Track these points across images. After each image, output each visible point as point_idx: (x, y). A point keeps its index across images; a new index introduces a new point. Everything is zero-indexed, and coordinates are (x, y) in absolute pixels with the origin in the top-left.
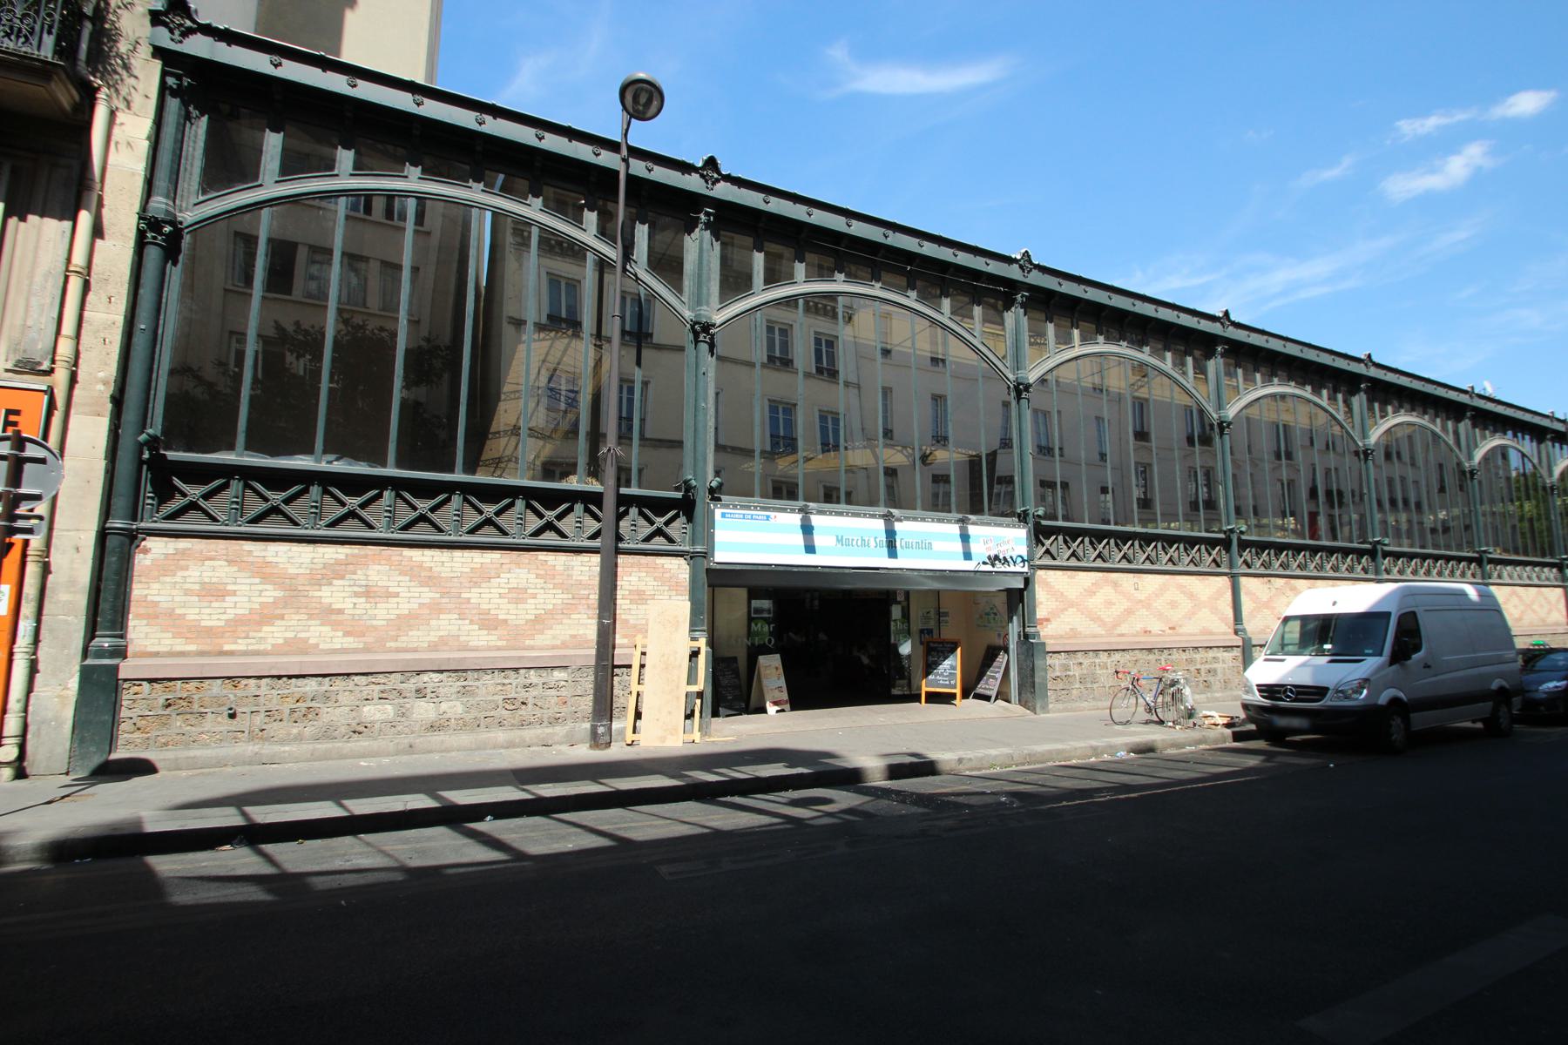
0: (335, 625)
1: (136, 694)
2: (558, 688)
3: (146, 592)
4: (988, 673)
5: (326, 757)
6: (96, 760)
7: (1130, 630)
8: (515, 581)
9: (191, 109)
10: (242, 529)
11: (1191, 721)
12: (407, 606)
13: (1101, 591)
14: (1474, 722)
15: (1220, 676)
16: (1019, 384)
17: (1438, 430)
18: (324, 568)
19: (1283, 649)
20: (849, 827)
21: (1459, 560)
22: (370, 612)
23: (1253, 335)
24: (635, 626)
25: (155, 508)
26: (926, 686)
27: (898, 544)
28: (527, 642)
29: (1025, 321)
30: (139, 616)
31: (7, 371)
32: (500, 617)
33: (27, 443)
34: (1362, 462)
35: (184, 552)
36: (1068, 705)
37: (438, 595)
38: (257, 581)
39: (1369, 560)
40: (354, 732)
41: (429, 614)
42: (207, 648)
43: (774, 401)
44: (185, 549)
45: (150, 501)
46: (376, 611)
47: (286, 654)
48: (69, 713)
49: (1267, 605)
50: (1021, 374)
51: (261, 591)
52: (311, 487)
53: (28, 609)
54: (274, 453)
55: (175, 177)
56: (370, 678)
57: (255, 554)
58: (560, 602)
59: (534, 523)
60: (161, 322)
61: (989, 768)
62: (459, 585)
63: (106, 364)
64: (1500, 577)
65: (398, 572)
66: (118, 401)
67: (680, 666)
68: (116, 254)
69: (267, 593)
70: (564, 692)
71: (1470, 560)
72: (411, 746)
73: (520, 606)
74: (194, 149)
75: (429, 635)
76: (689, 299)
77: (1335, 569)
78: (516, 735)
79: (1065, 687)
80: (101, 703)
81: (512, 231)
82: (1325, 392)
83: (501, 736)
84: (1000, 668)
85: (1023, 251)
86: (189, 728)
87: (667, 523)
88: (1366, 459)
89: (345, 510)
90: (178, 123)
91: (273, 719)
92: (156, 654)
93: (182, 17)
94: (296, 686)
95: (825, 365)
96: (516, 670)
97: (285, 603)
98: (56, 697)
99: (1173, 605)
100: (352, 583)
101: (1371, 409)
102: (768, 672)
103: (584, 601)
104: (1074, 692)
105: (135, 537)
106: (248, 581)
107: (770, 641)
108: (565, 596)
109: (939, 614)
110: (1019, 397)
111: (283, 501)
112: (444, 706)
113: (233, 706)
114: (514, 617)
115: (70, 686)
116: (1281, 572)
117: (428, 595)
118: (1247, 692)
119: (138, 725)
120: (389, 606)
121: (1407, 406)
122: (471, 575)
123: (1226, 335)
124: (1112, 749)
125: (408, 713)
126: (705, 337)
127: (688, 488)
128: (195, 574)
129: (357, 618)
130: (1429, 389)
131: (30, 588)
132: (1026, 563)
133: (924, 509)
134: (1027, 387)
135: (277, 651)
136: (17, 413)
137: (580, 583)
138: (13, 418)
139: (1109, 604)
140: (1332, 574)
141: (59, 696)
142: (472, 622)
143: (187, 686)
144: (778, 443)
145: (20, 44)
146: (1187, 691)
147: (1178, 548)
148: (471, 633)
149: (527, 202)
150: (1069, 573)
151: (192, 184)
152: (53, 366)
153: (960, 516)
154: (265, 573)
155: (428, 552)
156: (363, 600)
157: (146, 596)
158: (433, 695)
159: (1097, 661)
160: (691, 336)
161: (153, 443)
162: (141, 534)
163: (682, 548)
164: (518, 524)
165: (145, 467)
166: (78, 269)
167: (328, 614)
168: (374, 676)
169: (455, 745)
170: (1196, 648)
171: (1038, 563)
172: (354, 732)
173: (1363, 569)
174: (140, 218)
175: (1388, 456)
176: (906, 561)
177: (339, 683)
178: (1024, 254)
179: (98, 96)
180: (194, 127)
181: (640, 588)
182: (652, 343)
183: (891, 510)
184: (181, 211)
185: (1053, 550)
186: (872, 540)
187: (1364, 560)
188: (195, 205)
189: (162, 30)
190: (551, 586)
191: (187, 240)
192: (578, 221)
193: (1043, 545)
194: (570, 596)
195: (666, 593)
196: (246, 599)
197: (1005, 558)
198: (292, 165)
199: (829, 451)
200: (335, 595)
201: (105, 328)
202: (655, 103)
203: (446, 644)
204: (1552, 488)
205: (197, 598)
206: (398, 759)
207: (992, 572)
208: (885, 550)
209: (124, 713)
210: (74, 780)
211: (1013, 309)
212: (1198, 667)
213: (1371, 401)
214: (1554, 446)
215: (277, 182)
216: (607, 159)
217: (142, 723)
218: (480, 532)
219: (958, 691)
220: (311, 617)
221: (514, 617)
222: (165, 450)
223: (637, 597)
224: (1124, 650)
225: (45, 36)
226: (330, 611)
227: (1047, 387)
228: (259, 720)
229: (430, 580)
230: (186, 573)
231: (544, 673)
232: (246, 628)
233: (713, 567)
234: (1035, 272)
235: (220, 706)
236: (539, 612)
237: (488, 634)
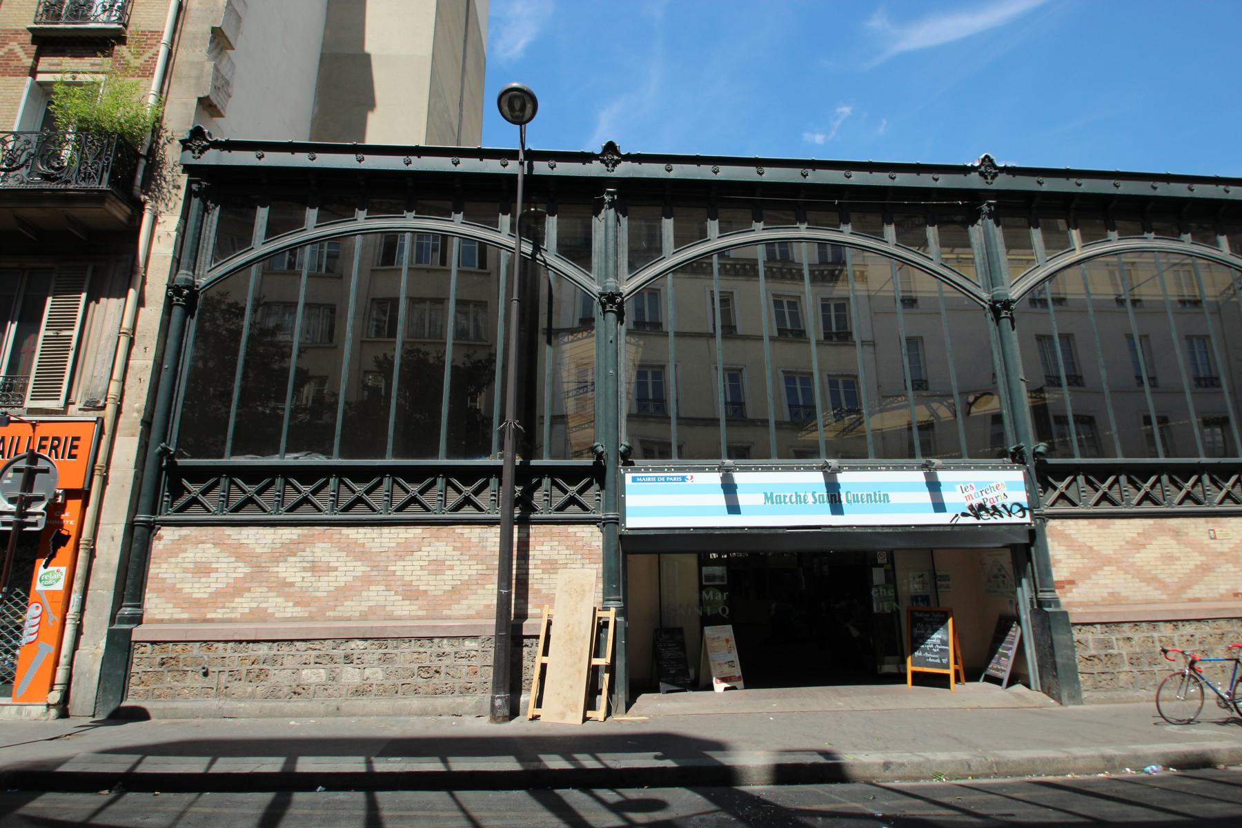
0: (288, 596)
1: (142, 653)
2: (469, 657)
4: (1000, 650)
5: (270, 715)
8: (435, 553)
9: (208, 203)
12: (344, 579)
13: (1154, 542)
16: (995, 302)
18: (282, 547)
22: (315, 584)
27: (843, 498)
28: (446, 612)
29: (998, 233)
30: (152, 590)
32: (422, 588)
33: (39, 459)
36: (1114, 694)
37: (369, 569)
38: (233, 559)
40: (295, 693)
41: (361, 586)
42: (195, 616)
43: (789, 372)
44: (186, 536)
45: (166, 499)
46: (320, 584)
48: (97, 667)
50: (999, 291)
51: (236, 568)
53: (77, 585)
56: (309, 645)
57: (233, 537)
59: (453, 498)
61: (931, 778)
67: (584, 638)
68: (152, 315)
72: (338, 709)
73: (439, 577)
79: (1107, 670)
80: (119, 660)
83: (415, 703)
84: (1012, 643)
85: (983, 156)
86: (176, 683)
87: (580, 492)
90: (198, 215)
91: (235, 678)
92: (161, 621)
94: (252, 650)
95: (834, 330)
96: (431, 639)
100: (301, 559)
102: (716, 644)
105: (153, 528)
106: (226, 560)
107: (724, 610)
108: (480, 567)
111: (256, 493)
112: (368, 672)
113: (206, 666)
114: (433, 588)
117: (360, 568)
120: (330, 579)
122: (396, 549)
124: (1139, 761)
126: (611, 307)
128: (191, 555)
129: (304, 589)
131: (80, 571)
132: (1027, 513)
133: (878, 456)
135: (245, 619)
136: (78, 439)
138: (76, 443)
141: (93, 654)
142: (397, 593)
148: (396, 603)
155: (362, 530)
156: (309, 574)
157: (158, 574)
158: (358, 661)
159: (1156, 635)
167: (283, 587)
174: (168, 288)
176: (854, 517)
177: (285, 648)
178: (983, 160)
180: (210, 216)
183: (828, 461)
185: (1071, 494)
188: (209, 271)
189: (189, 153)
190: (467, 557)
192: (1215, 244)
193: (1055, 488)
195: (578, 561)
197: (994, 508)
198: (682, 241)
200: (289, 571)
202: (529, 107)
203: (374, 613)
205: (190, 575)
206: (325, 720)
207: (977, 525)
208: (827, 505)
209: (134, 669)
211: (980, 222)
215: (263, 244)
217: (145, 678)
218: (189, 510)
220: (270, 589)
221: (433, 588)
224: (1199, 620)
225: (105, 173)
227: (1066, 305)
228: (224, 678)
229: (361, 554)
230: (184, 555)
231: (456, 642)
233: (625, 533)
235: (198, 665)
236: (455, 583)
237: (410, 605)
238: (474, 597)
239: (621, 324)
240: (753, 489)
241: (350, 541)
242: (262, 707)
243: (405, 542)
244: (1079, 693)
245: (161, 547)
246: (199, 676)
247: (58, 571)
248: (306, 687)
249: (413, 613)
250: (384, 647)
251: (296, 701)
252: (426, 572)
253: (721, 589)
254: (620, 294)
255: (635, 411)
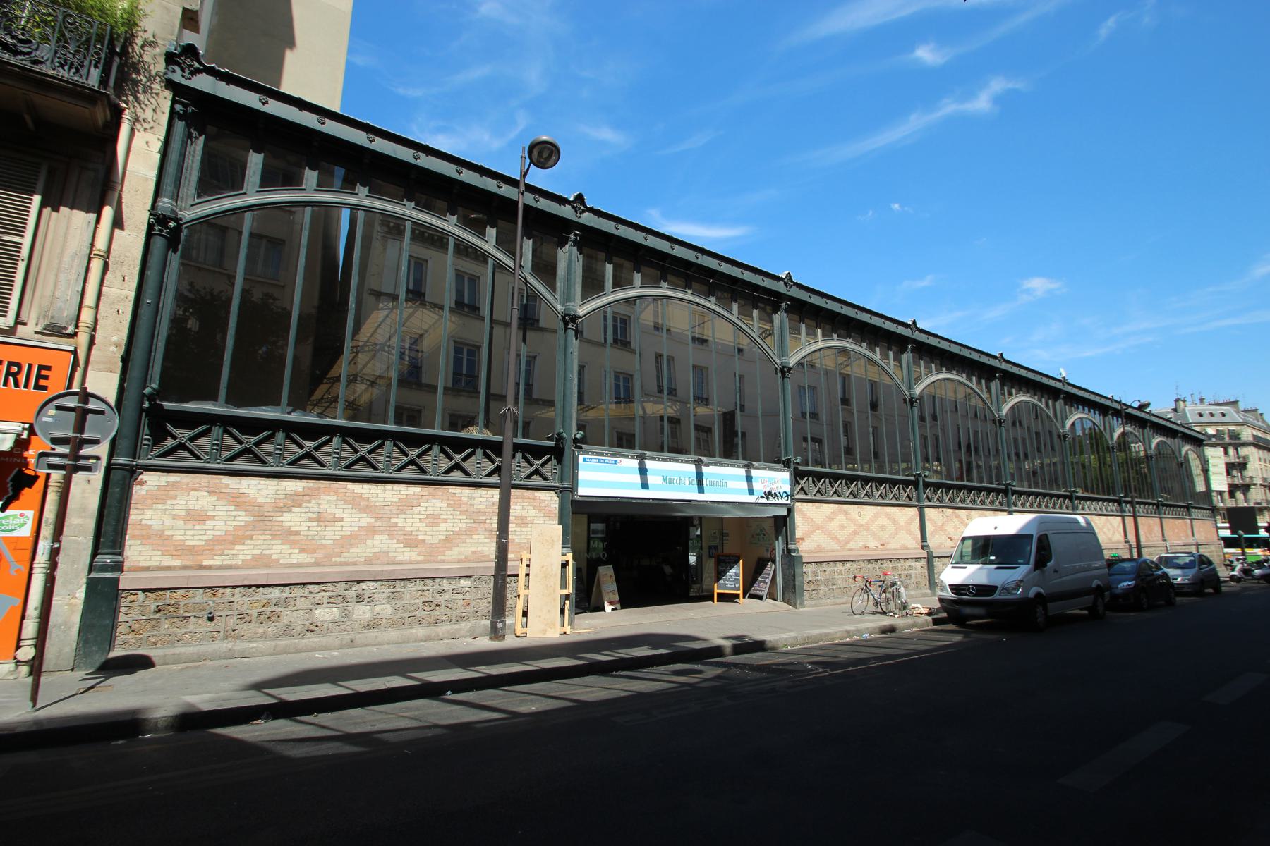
0: (293, 544)
2: (463, 593)
3: (141, 517)
4: (760, 579)
6: (99, 660)
7: (856, 546)
9: (192, 130)
10: (221, 466)
11: (905, 611)
12: (349, 528)
14: (1081, 609)
15: (913, 579)
16: (784, 367)
17: (1043, 406)
18: (286, 498)
19: (961, 559)
20: (722, 687)
21: (1058, 496)
22: (320, 533)
23: (931, 338)
24: (519, 544)
25: (150, 448)
26: (718, 589)
28: (440, 557)
29: (786, 321)
30: (133, 537)
31: (36, 333)
32: (420, 537)
33: (90, 398)
34: (998, 428)
35: (173, 484)
37: (373, 520)
38: (232, 508)
39: (1004, 496)
40: (308, 631)
42: (189, 563)
43: (618, 372)
47: (254, 568)
48: (76, 618)
49: (941, 528)
50: (785, 359)
51: (235, 517)
52: (277, 434)
53: (47, 531)
54: (239, 406)
55: (178, 183)
56: (321, 587)
58: (464, 525)
59: (445, 464)
60: (162, 297)
62: (389, 512)
63: (119, 330)
64: (1083, 509)
65: (343, 502)
66: (125, 359)
67: (555, 575)
68: (131, 243)
69: (240, 518)
70: (468, 596)
71: (1065, 497)
72: (352, 641)
74: (193, 162)
75: (365, 551)
76: (560, 296)
77: (983, 502)
78: (432, 630)
80: (104, 609)
81: (380, 222)
82: (974, 378)
83: (421, 632)
84: (769, 575)
85: (787, 272)
86: (175, 629)
88: (1000, 426)
89: (303, 452)
90: (183, 141)
92: (148, 569)
93: (192, 60)
96: (432, 579)
97: (254, 526)
98: (66, 605)
99: (883, 527)
101: (1002, 389)
103: (482, 525)
104: (821, 592)
105: (134, 472)
106: (225, 508)
108: (468, 521)
109: (722, 534)
110: (783, 377)
112: (377, 609)
115: (77, 595)
116: (950, 504)
117: (365, 520)
118: (942, 590)
119: (133, 628)
121: (1024, 389)
123: (1001, 367)
124: (859, 632)
125: (349, 615)
126: (572, 326)
127: (560, 438)
128: (182, 502)
129: (310, 538)
130: (1038, 378)
133: (611, 445)
134: (789, 369)
135: (246, 565)
136: (49, 368)
137: (479, 511)
138: (44, 373)
139: (842, 527)
140: (980, 506)
142: (398, 541)
143: (175, 594)
144: (459, 380)
145: (71, 74)
146: (902, 590)
147: (885, 487)
149: (446, 219)
150: (817, 504)
151: (190, 189)
152: (76, 330)
153: (696, 458)
154: (238, 502)
155: (366, 486)
156: (315, 524)
159: (836, 569)
160: (562, 324)
161: (151, 398)
162: (139, 469)
163: (553, 484)
164: (434, 464)
165: (144, 414)
166: (101, 253)
167: (288, 536)
168: (325, 585)
169: (386, 639)
170: (898, 559)
171: (796, 497)
172: (308, 631)
173: (1000, 503)
174: (151, 214)
175: (1014, 424)
176: (709, 496)
177: (297, 591)
179: (124, 116)
181: (523, 515)
182: (480, 315)
184: (181, 210)
186: (687, 479)
187: (1000, 497)
188: (192, 205)
191: (185, 232)
192: (481, 234)
193: (799, 484)
194: (472, 521)
195: (541, 518)
196: (223, 523)
197: (775, 493)
198: (269, 180)
199: (620, 403)
200: (293, 520)
201: (119, 301)
204: (1113, 448)
205: (182, 522)
207: (767, 504)
209: (122, 618)
210: (87, 674)
211: (779, 313)
212: (900, 573)
213: (1002, 385)
214: (1113, 419)
215: (257, 192)
216: (506, 191)
217: (136, 626)
218: (173, 456)
219: (740, 592)
220: (274, 537)
221: (430, 537)
222: (161, 401)
223: (520, 522)
224: (852, 561)
225: (92, 69)
226: (290, 532)
227: (708, 346)
228: (232, 622)
229: (367, 508)
230: (174, 502)
231: (453, 581)
232: (223, 547)
234: (794, 288)
236: (448, 533)
237: (410, 551)
238: (464, 545)
239: (175, 251)
240: (656, 472)
241: (356, 495)
242: (276, 646)
243: (406, 498)
244: (803, 601)
245: (144, 492)
246: (204, 621)
247: (22, 515)
248: (319, 625)
249: (413, 558)
250: (392, 587)
251: (309, 638)
252: (424, 524)
253: (602, 540)
254: (177, 220)
255: (450, 385)
